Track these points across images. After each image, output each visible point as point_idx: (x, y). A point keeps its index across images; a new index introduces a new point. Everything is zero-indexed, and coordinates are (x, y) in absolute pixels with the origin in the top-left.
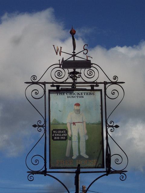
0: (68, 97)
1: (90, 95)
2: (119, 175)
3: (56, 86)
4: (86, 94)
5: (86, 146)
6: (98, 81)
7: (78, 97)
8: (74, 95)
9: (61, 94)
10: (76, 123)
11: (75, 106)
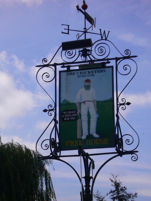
0: (79, 76)
1: (101, 72)
2: (130, 156)
3: (67, 67)
4: (97, 72)
5: (105, 148)
6: (109, 57)
7: (89, 76)
8: (85, 74)
9: (71, 74)
10: (86, 101)
11: (86, 83)
